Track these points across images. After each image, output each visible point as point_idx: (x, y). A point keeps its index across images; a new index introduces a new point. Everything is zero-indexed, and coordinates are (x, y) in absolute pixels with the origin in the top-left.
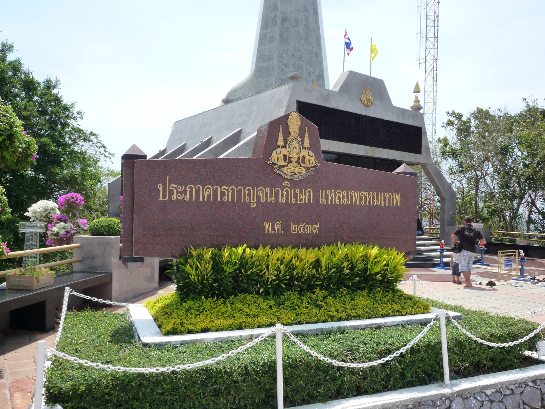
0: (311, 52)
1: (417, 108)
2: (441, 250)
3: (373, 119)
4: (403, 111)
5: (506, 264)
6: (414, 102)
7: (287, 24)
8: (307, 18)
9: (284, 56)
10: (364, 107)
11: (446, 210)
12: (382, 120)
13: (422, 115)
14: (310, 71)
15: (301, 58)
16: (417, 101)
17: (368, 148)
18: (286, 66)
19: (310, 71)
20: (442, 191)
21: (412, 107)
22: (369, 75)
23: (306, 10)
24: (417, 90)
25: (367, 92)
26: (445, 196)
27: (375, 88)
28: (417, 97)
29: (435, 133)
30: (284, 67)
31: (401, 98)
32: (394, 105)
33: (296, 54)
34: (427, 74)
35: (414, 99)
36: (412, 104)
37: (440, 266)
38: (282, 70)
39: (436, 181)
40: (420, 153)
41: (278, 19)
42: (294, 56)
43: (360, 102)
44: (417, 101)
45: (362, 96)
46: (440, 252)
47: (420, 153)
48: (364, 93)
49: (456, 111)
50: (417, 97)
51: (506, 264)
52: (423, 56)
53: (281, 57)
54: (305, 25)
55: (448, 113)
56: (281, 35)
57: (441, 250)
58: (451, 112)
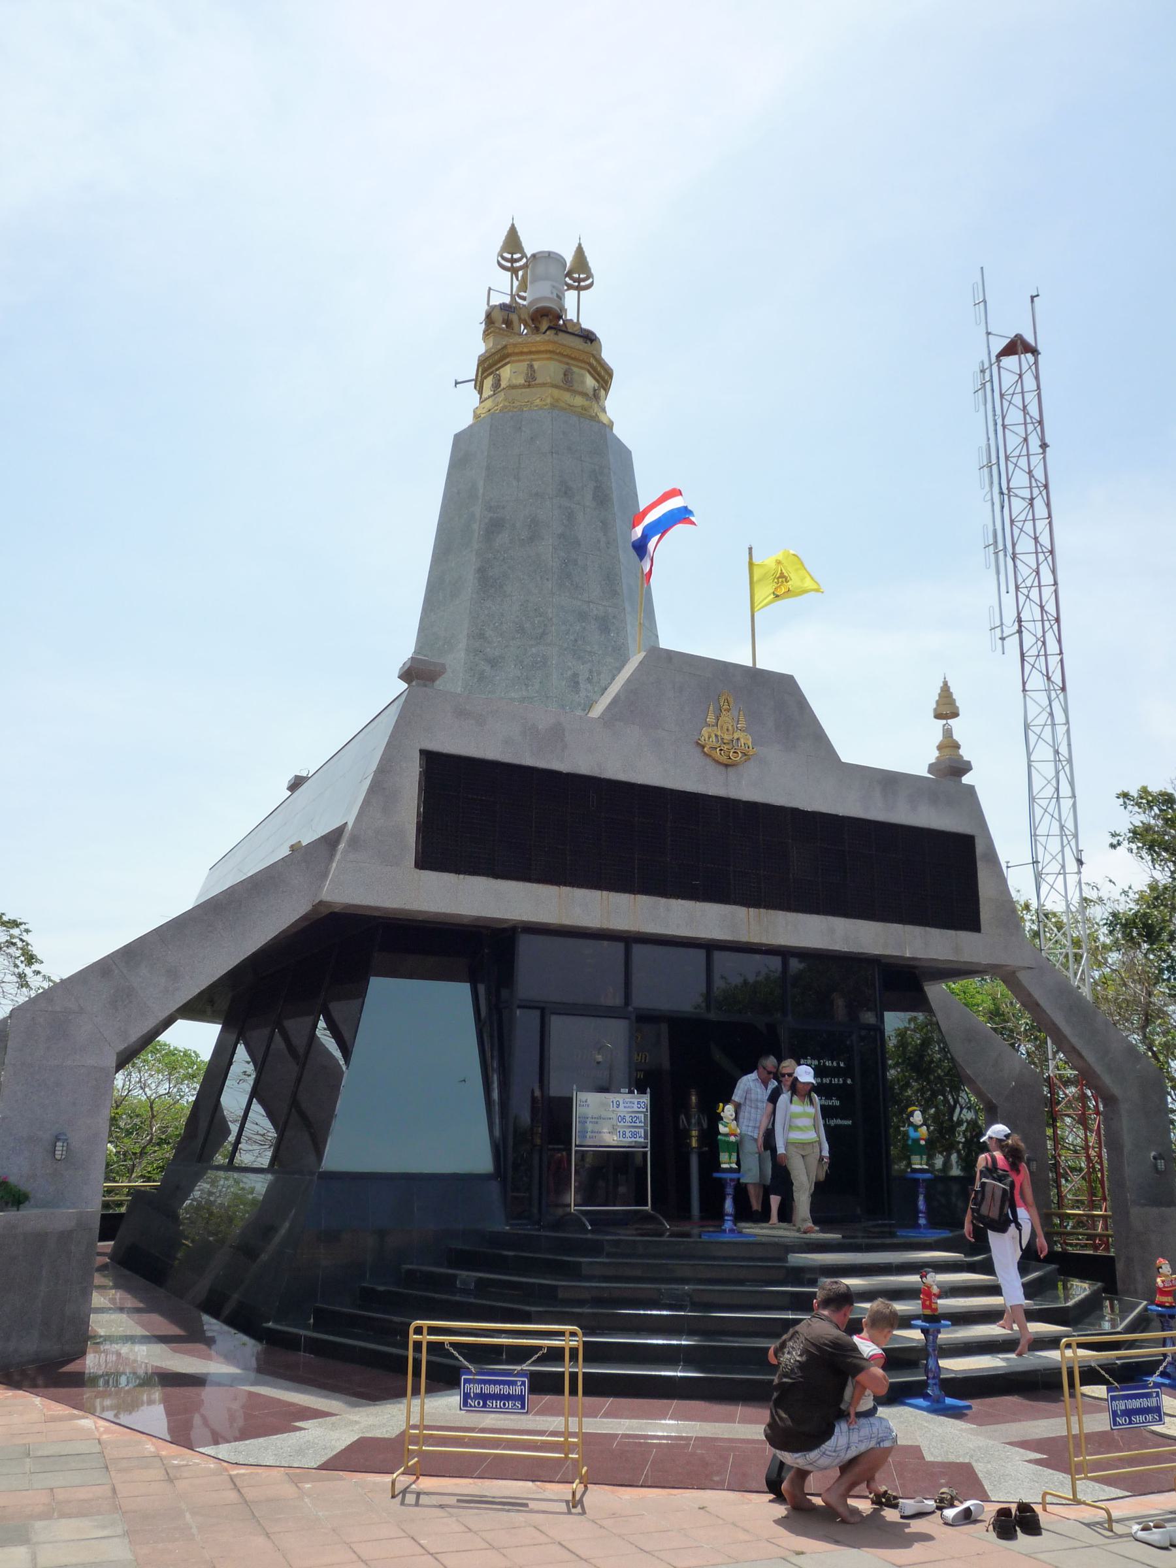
0: (583, 616)
1: (952, 765)
2: (926, 1318)
3: (754, 808)
4: (890, 781)
5: (1121, 1405)
6: (940, 748)
7: (503, 538)
8: (571, 516)
9: (489, 633)
10: (711, 768)
11: (1128, 1145)
12: (795, 812)
13: (971, 790)
14: (575, 675)
15: (544, 634)
16: (949, 745)
17: (740, 912)
18: (494, 663)
19: (575, 675)
20: (1098, 1069)
21: (932, 768)
22: (742, 658)
23: (566, 491)
24: (946, 709)
25: (725, 718)
26: (1116, 1090)
27: (774, 702)
28: (948, 733)
29: (1080, 862)
30: (488, 668)
31: (874, 731)
32: (843, 760)
33: (527, 625)
34: (1027, 667)
35: (938, 737)
36: (933, 755)
37: (926, 1396)
38: (482, 677)
39: (1067, 1030)
40: (974, 925)
41: (475, 526)
42: (521, 630)
43: (699, 749)
44: (949, 745)
45: (705, 731)
46: (925, 1331)
47: (974, 925)
48: (711, 719)
49: (1154, 788)
50: (948, 733)
51: (1121, 1405)
52: (1010, 616)
53: (481, 636)
54: (562, 536)
55: (1125, 795)
56: (481, 571)
57: (926, 1318)
58: (1134, 793)
